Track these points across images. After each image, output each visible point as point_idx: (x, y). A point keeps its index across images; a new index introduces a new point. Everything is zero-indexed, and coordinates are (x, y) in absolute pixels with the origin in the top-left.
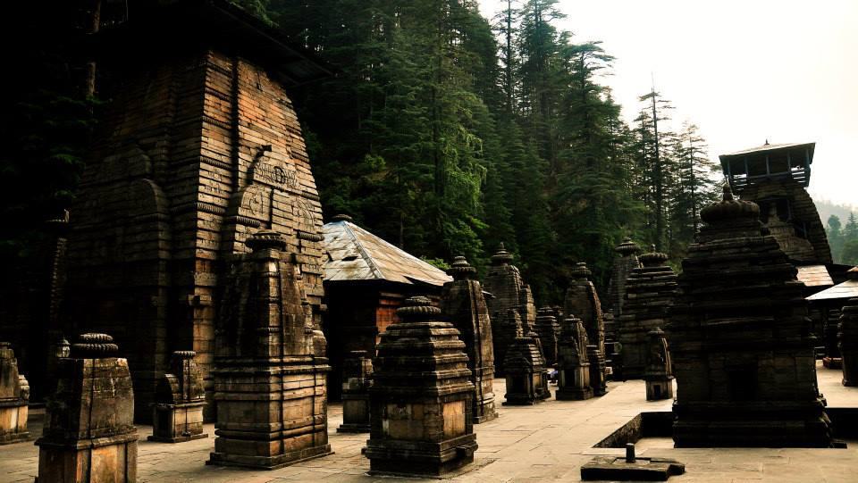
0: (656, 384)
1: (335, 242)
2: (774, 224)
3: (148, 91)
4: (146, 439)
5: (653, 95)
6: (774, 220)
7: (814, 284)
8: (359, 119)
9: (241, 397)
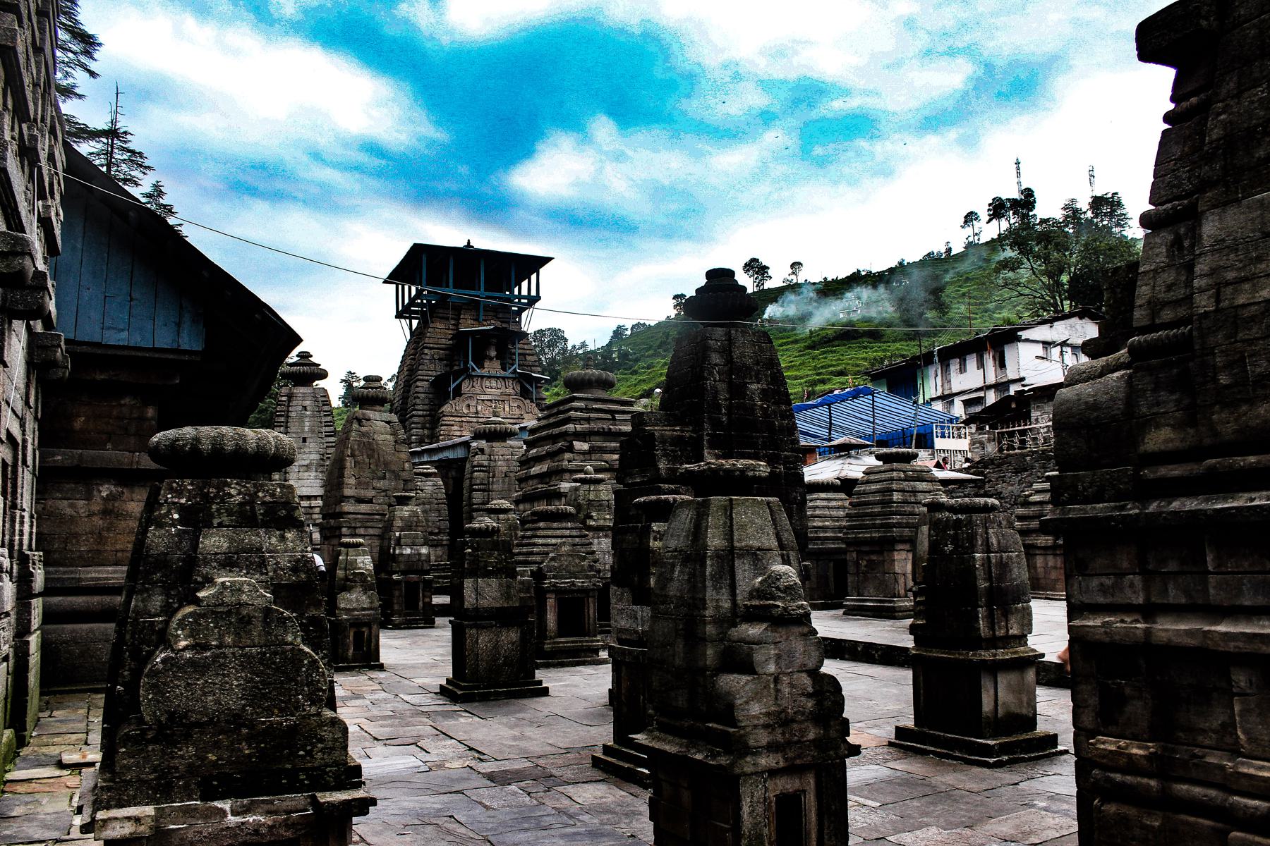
2: (493, 373)
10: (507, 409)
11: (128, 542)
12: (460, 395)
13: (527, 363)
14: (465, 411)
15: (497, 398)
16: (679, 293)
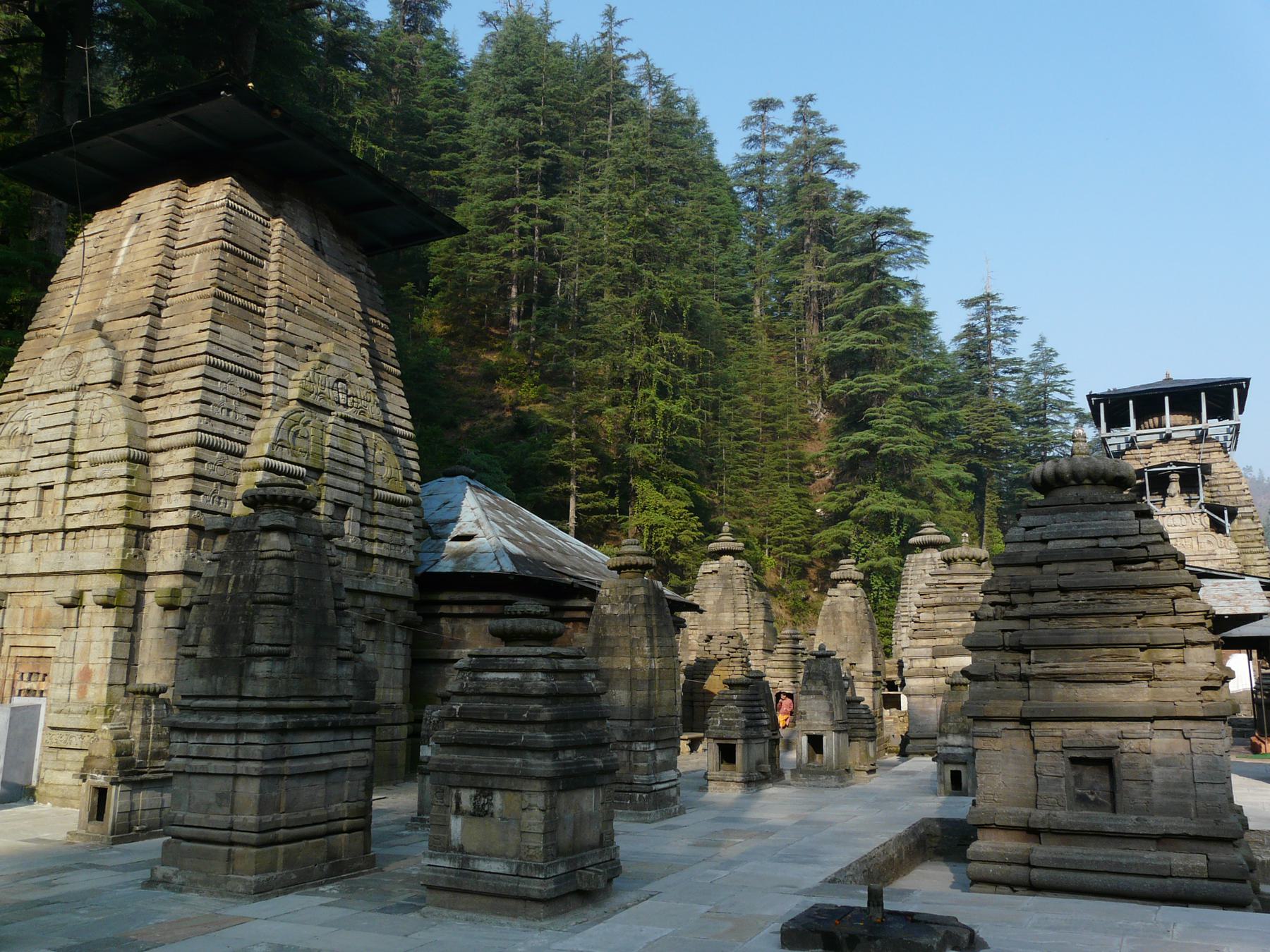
0: (954, 768)
1: (444, 510)
2: (1175, 510)
3: (126, 243)
4: (980, 833)
5: (988, 297)
6: (1176, 502)
7: (1240, 611)
8: (534, 308)
9: (213, 767)
10: (1195, 545)
13: (1231, 493)
15: (1182, 535)
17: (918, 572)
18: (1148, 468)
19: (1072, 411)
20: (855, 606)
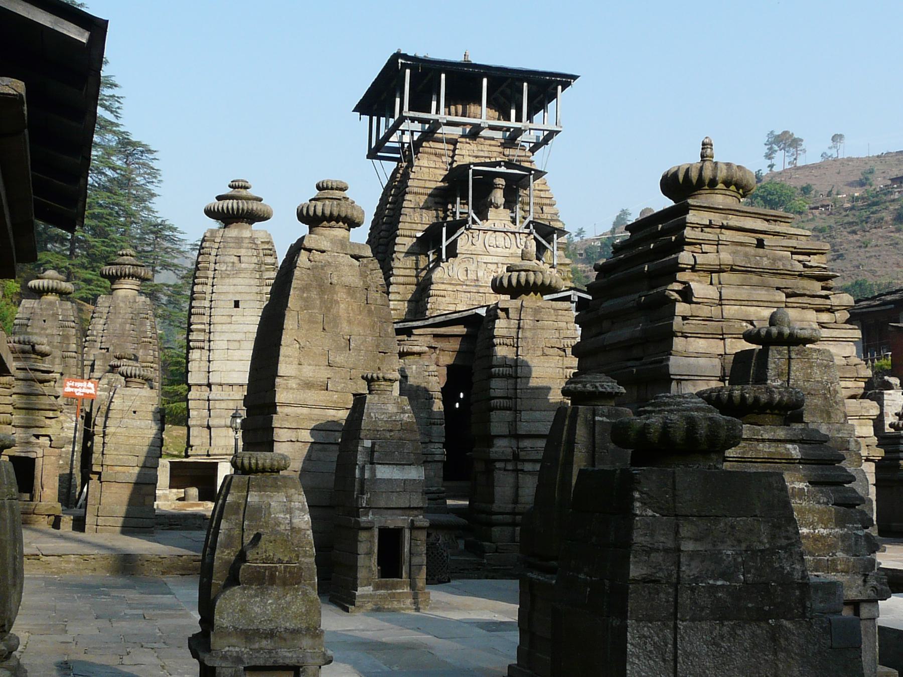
2: (499, 226)
11: (114, 434)
12: (455, 255)
14: (462, 277)
16: (614, 219)
17: (227, 259)
18: (476, 165)
19: (115, 133)
20: (363, 275)
